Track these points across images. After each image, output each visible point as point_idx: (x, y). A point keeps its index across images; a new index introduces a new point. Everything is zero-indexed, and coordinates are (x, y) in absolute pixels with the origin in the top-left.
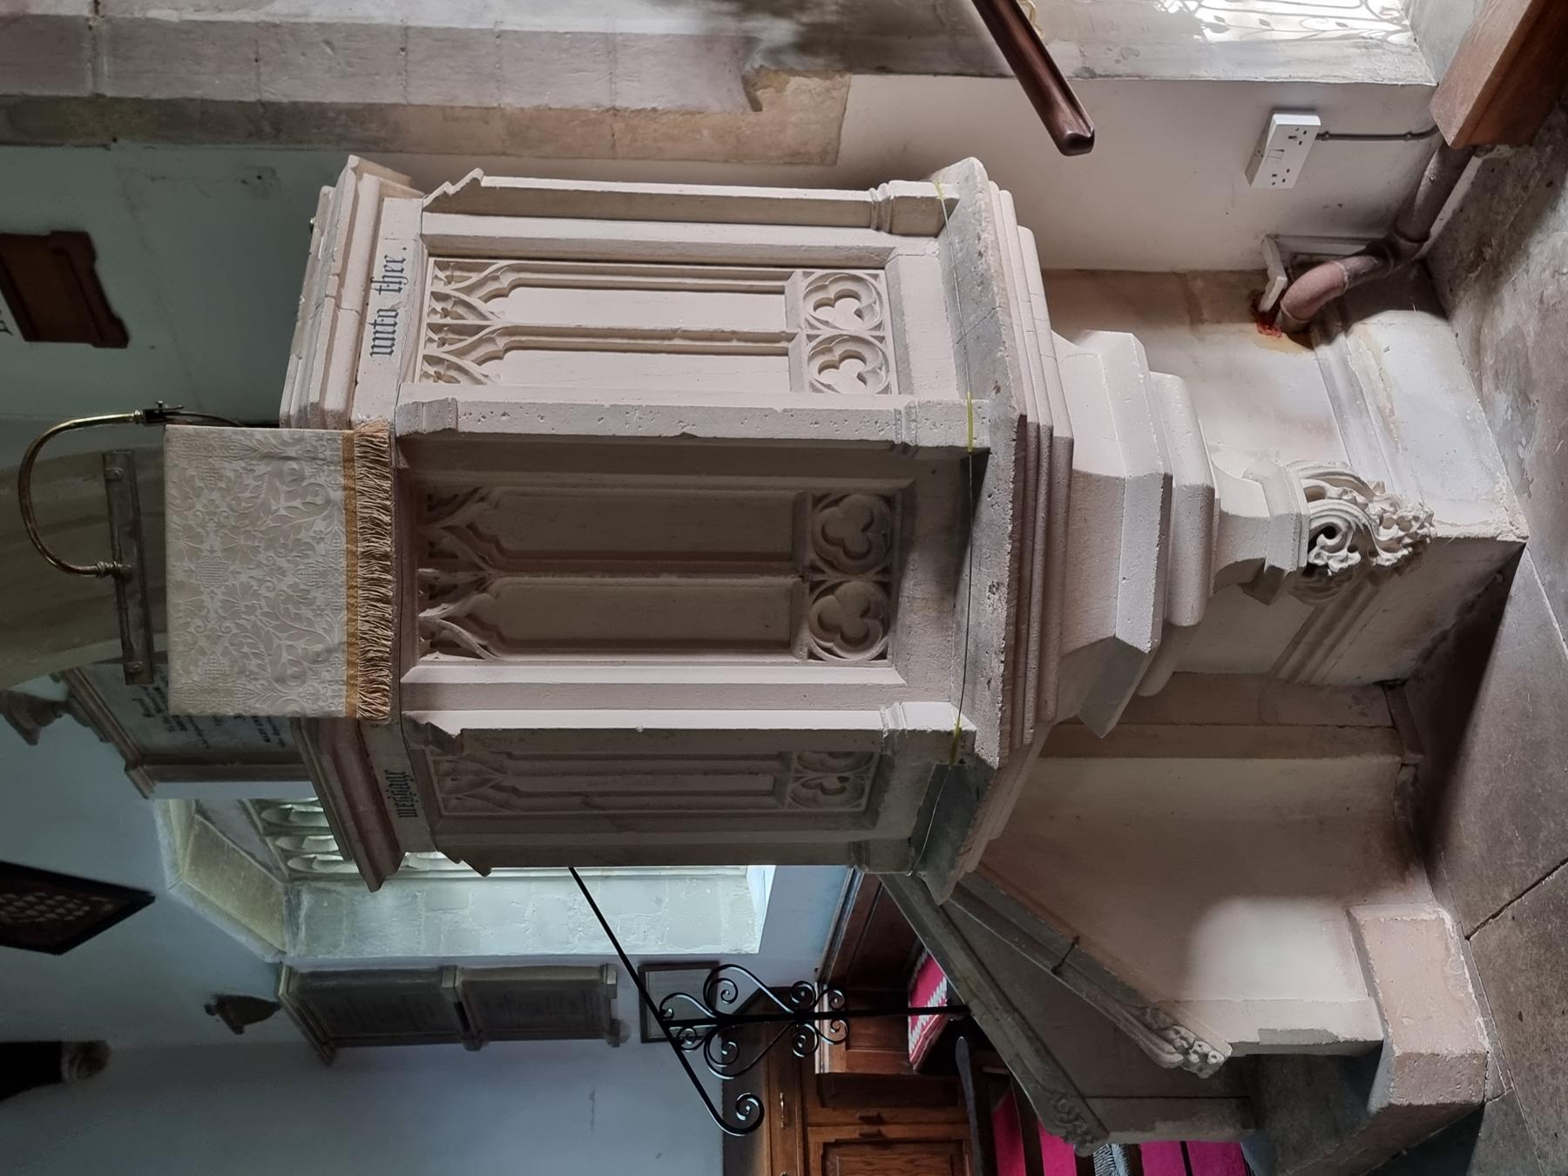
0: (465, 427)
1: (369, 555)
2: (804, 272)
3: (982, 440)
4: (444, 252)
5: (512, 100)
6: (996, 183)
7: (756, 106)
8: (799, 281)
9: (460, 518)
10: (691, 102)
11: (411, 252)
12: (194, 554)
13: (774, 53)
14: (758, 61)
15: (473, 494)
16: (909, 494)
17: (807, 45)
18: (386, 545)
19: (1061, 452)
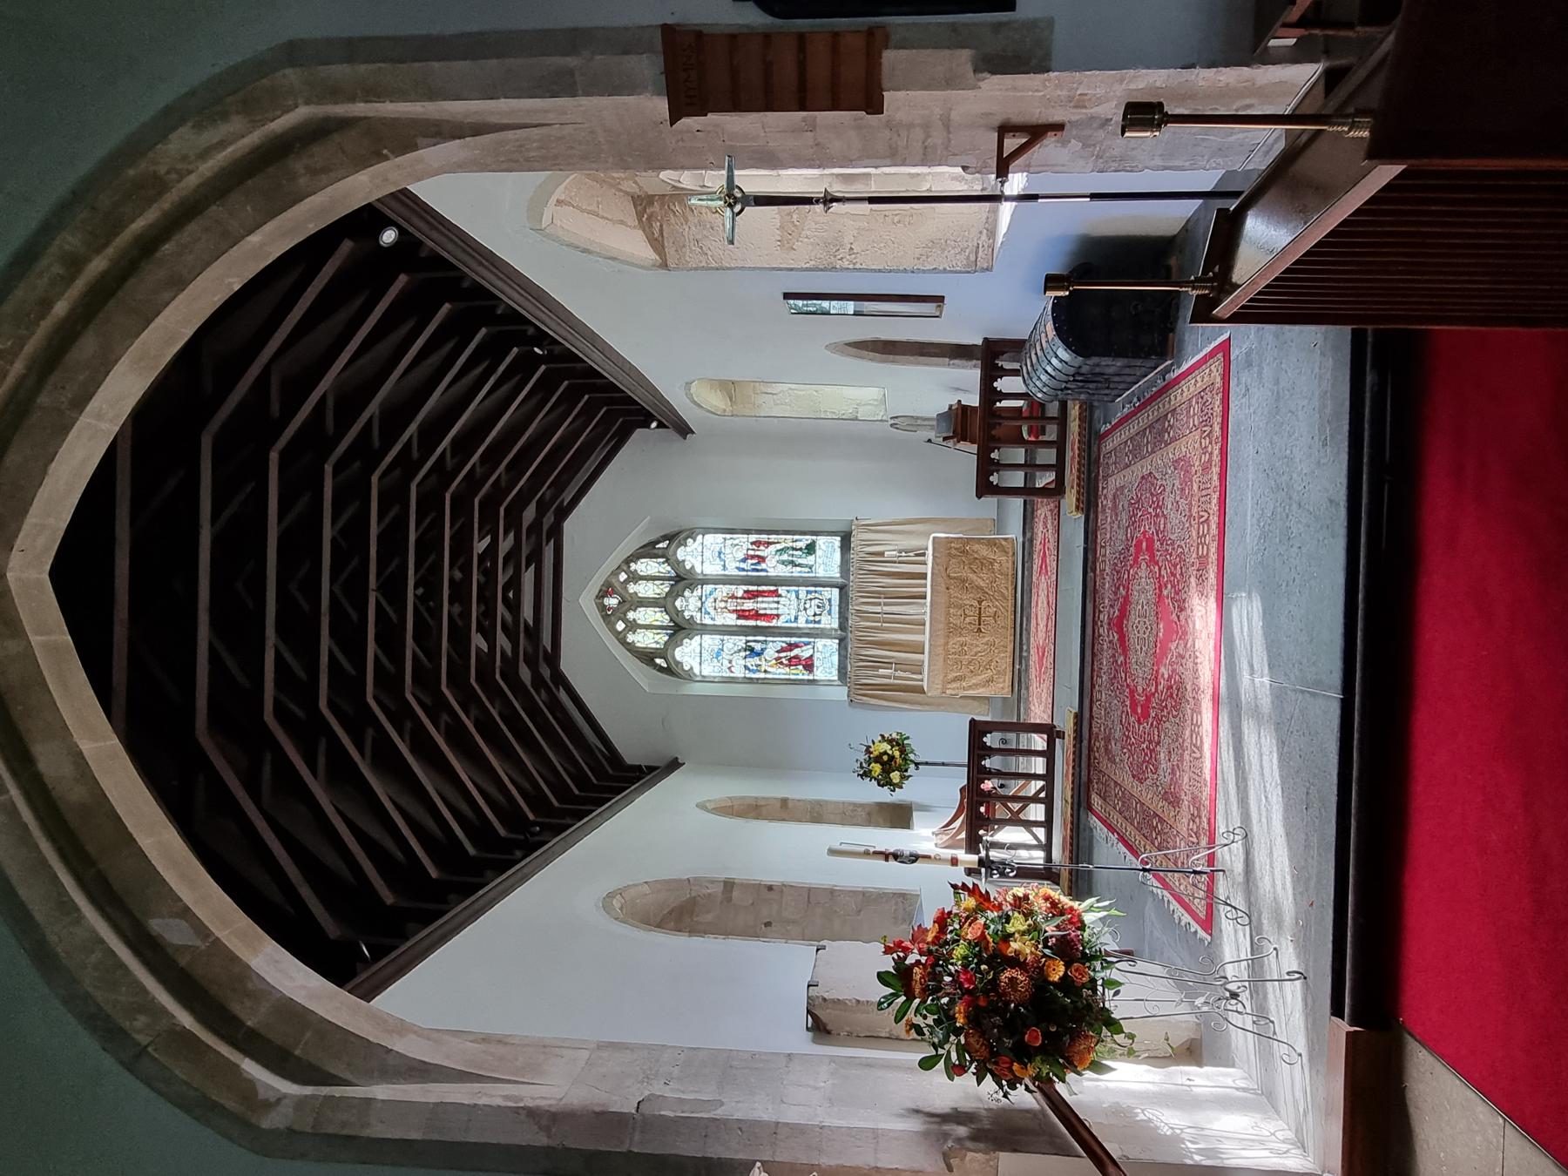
7: (950, 1169)
10: (916, 1166)
14: (950, 1144)
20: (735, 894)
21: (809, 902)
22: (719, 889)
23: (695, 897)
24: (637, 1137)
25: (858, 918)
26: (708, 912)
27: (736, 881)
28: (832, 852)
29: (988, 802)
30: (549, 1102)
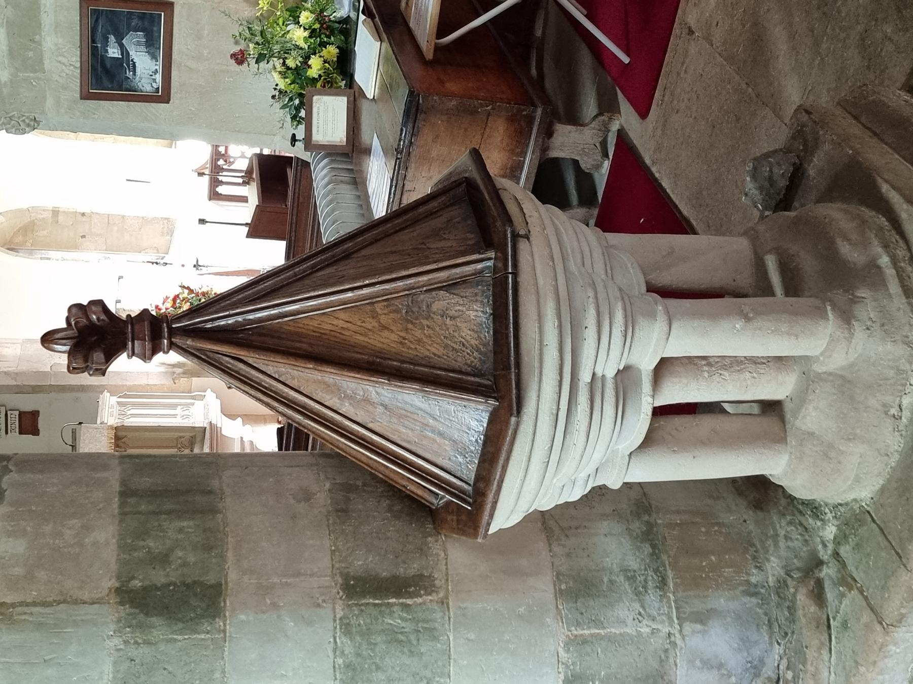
0: (125, 425)
1: (110, 443)
2: (157, 142)
3: (205, 426)
4: (118, 403)
5: (128, 383)
6: (579, 500)
7: (175, 383)
8: (179, 407)
9: (123, 440)
10: (162, 383)
11: (115, 404)
12: (84, 443)
13: (179, 374)
14: (175, 376)
15: (126, 436)
16: (195, 436)
17: (184, 373)
18: (113, 441)
19: (219, 429)
20: (61, 218)
21: (109, 223)
22: (49, 215)
23: (34, 221)
24: (52, 379)
25: (140, 233)
26: (43, 230)
27: (60, 209)
28: (127, 180)
29: (247, 177)
30: (13, 369)
